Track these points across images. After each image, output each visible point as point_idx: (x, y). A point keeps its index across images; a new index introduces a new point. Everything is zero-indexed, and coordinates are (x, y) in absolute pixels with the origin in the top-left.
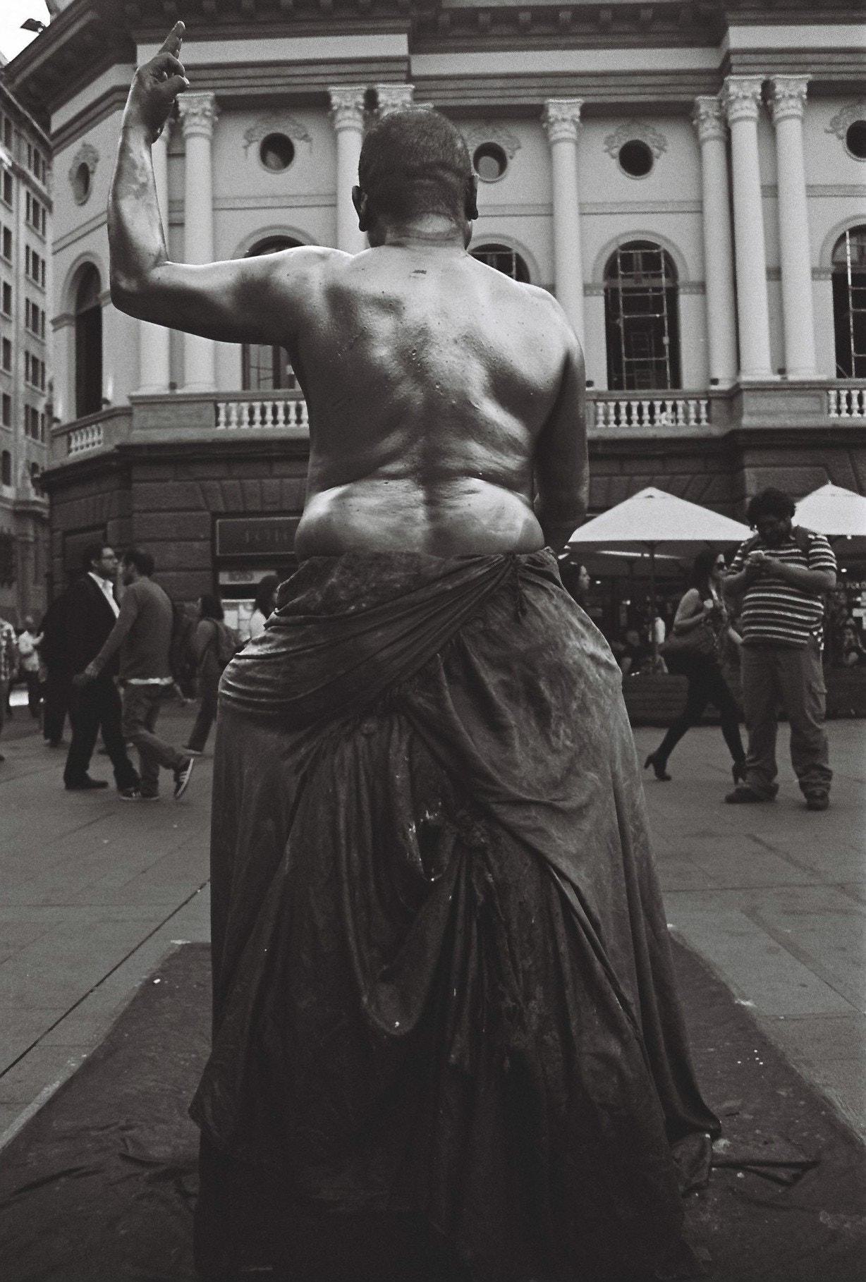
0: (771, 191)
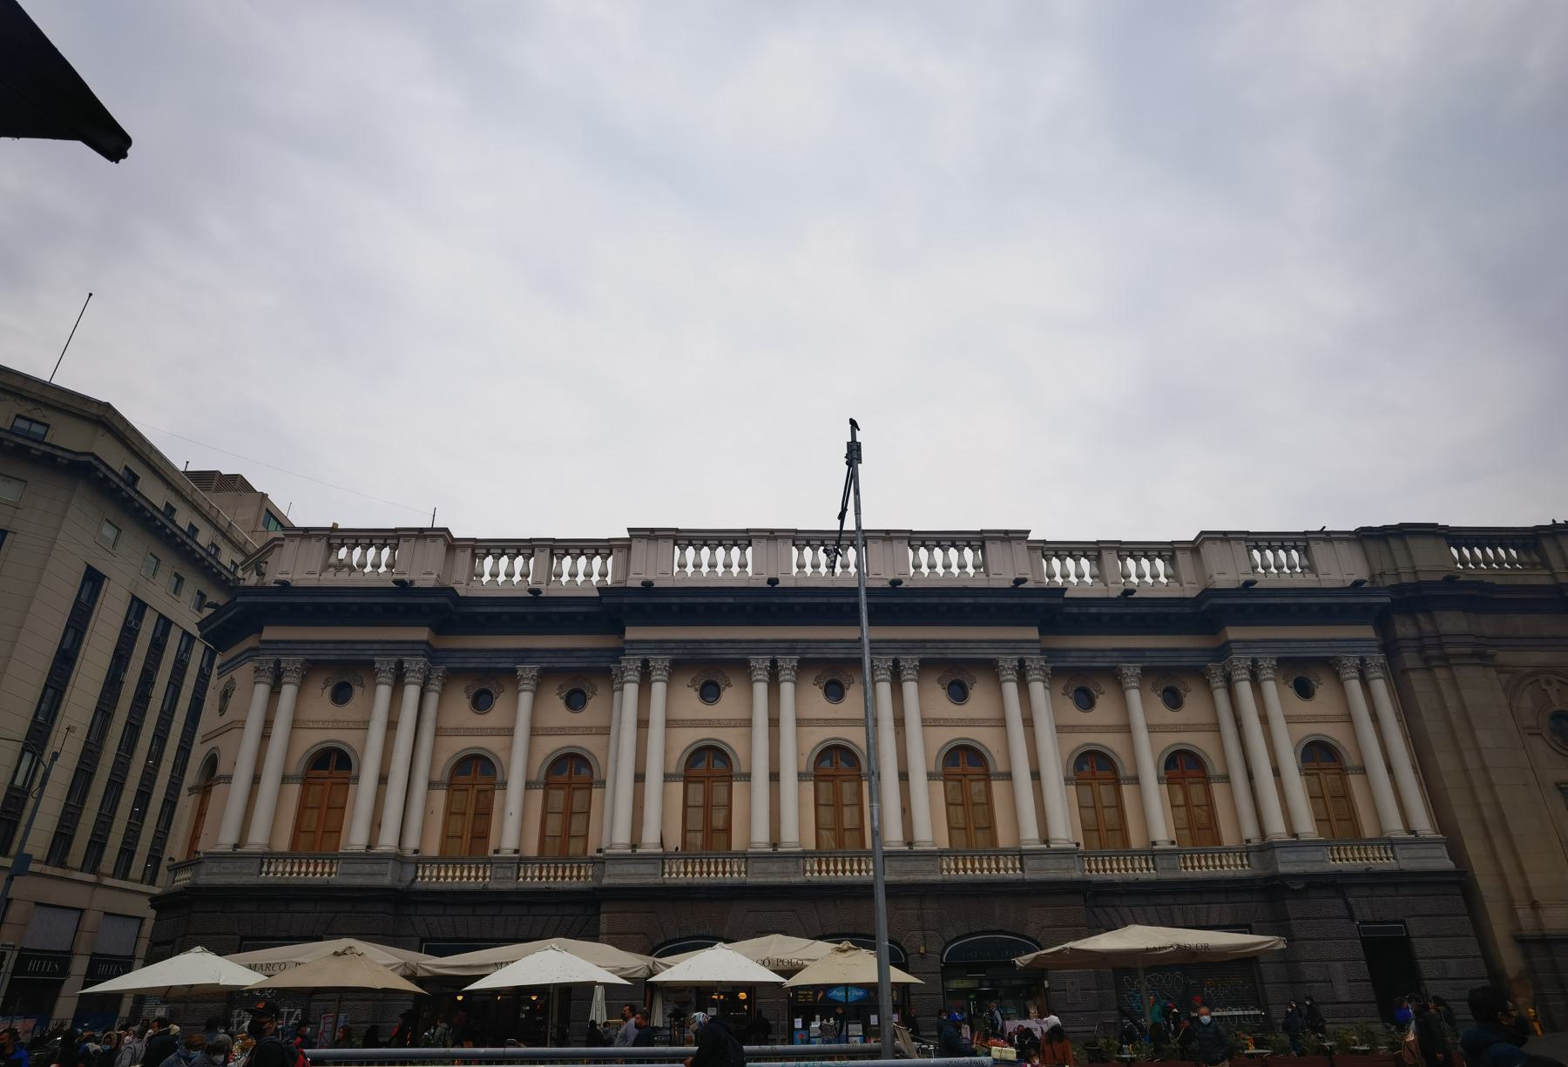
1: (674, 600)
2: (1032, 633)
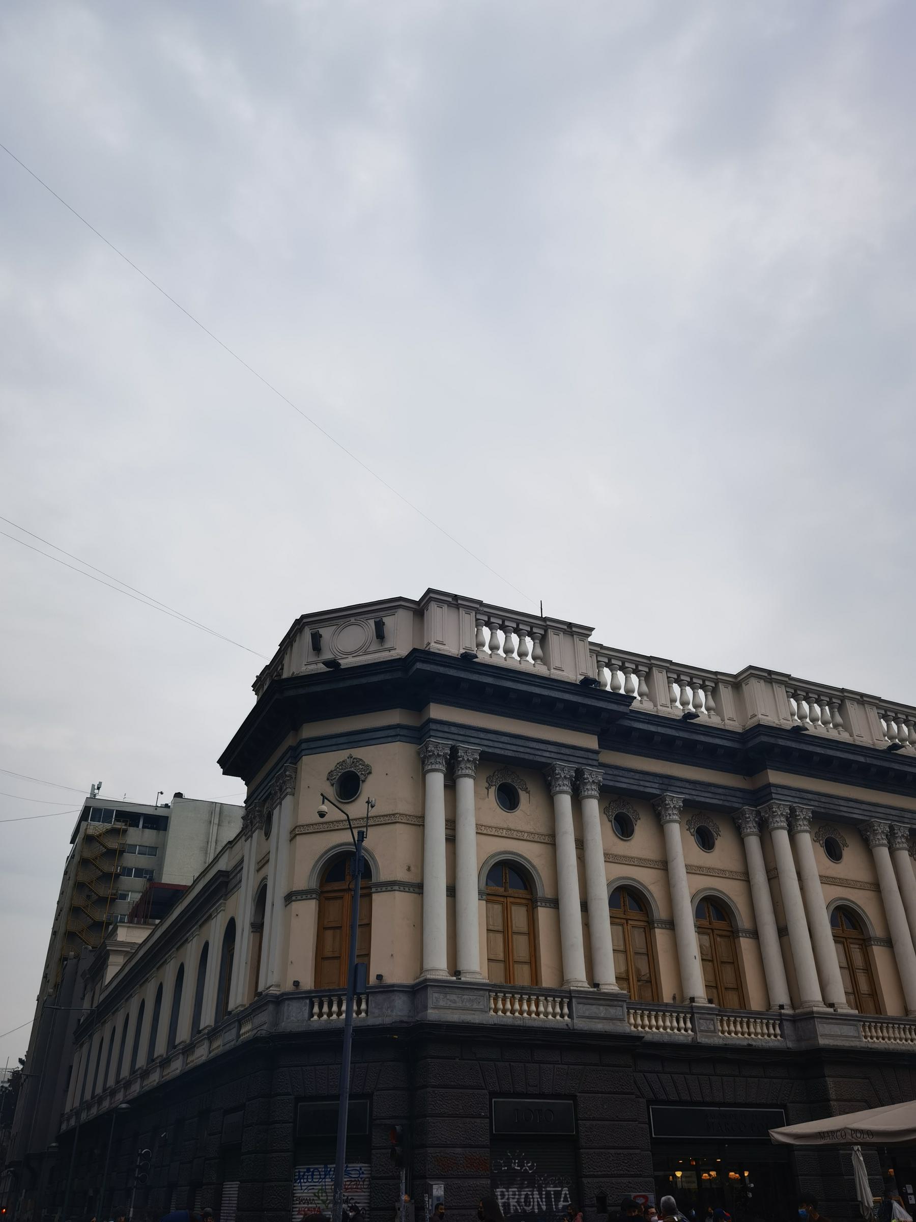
0: (452, 825)
1: (819, 750)
2: (591, 742)
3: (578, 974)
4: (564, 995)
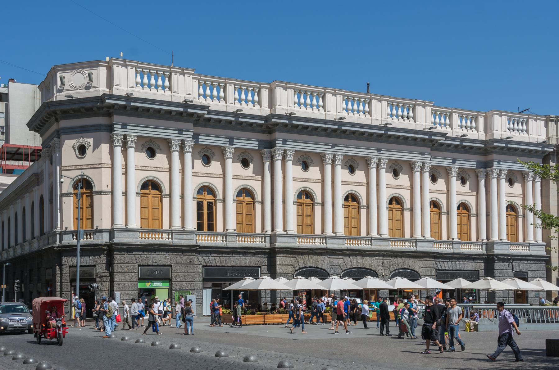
3: (329, 231)
4: (171, 232)
